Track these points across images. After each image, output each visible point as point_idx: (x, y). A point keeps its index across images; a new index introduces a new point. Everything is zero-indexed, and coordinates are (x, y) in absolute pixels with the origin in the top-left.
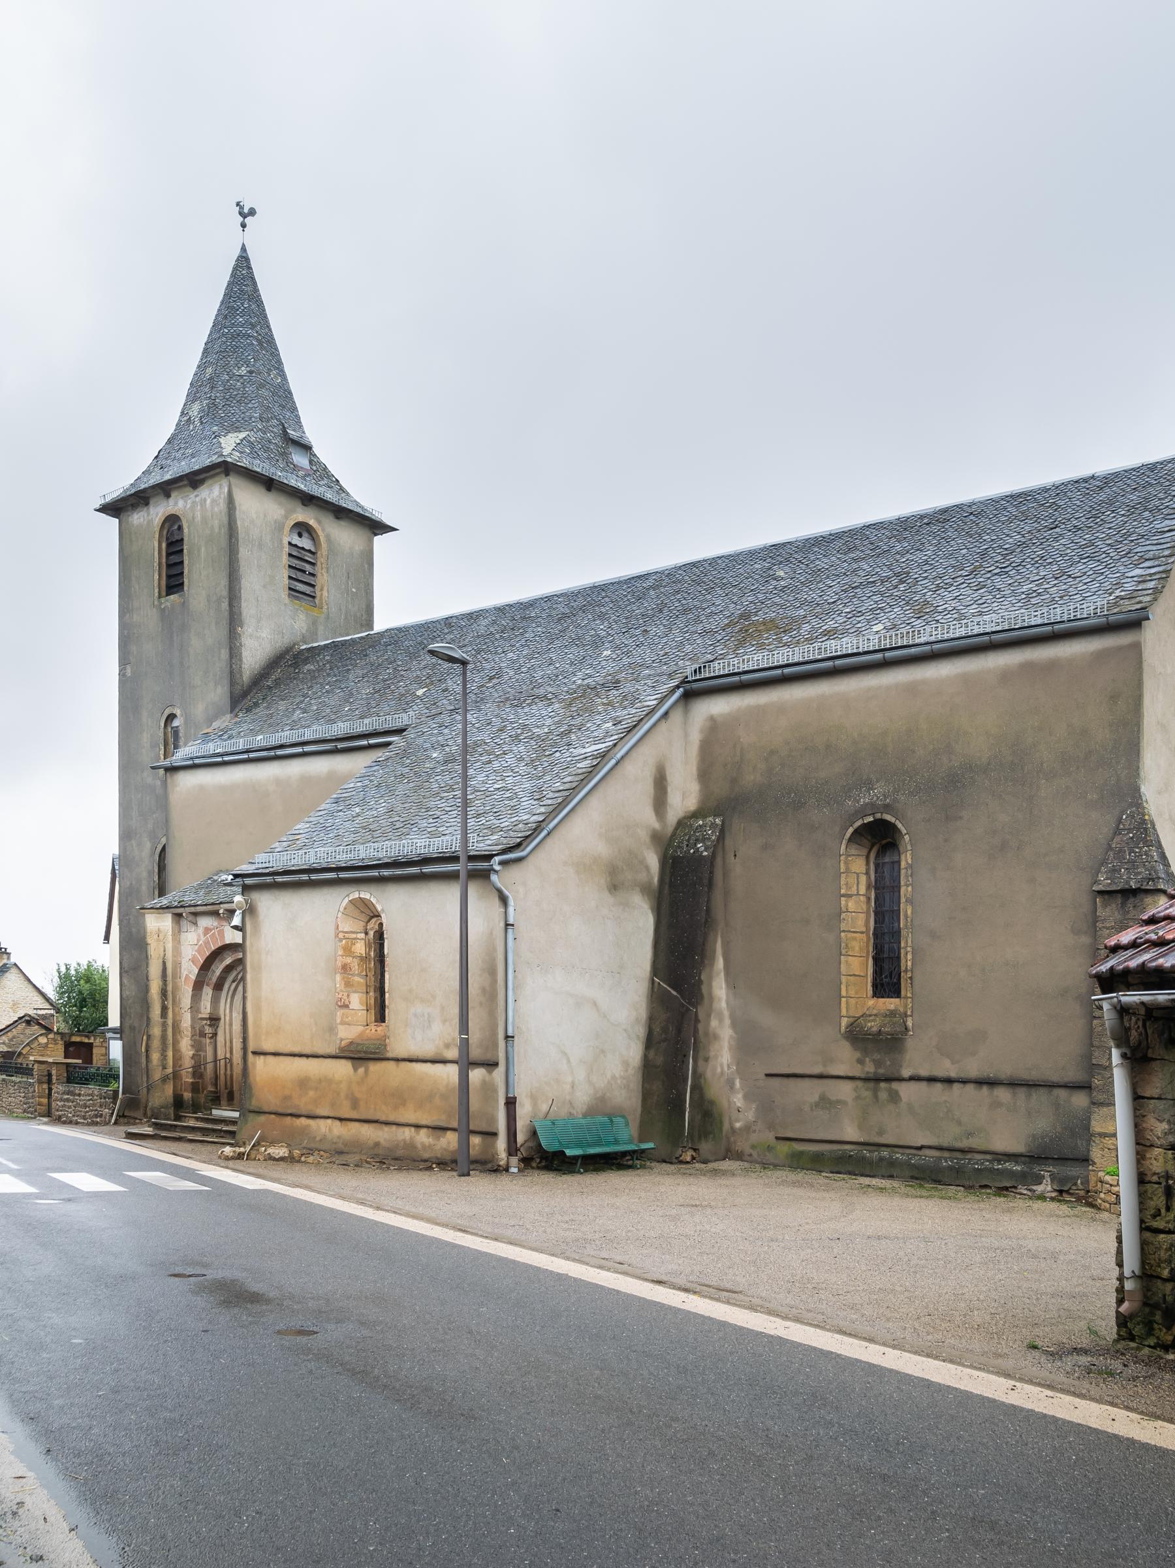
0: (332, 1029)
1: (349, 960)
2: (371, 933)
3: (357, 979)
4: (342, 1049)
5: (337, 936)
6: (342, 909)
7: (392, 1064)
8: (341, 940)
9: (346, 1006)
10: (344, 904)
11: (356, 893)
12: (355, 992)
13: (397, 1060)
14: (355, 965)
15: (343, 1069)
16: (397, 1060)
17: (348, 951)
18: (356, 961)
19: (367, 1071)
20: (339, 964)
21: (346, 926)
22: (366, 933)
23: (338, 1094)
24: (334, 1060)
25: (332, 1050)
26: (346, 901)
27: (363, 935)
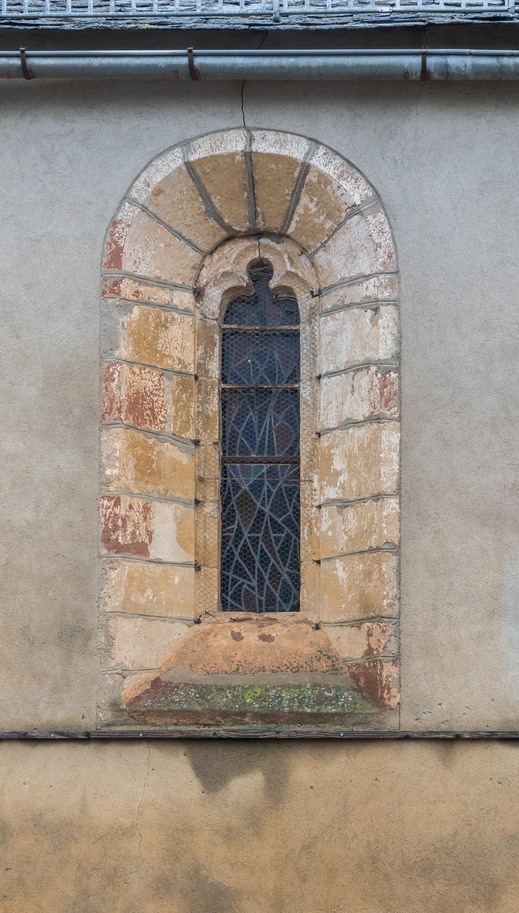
0: (75, 635)
1: (149, 381)
2: (215, 296)
3: (172, 452)
4: (134, 710)
5: (113, 289)
6: (141, 192)
7: (417, 759)
8: (126, 307)
9: (140, 549)
10: (158, 174)
11: (223, 137)
12: (166, 499)
13: (448, 740)
14: (167, 398)
15: (153, 785)
16: (448, 740)
17: (148, 352)
18: (169, 385)
19: (276, 788)
20: (122, 395)
21: (144, 257)
22: (198, 294)
23: (113, 878)
24: (86, 752)
25: (94, 715)
26: (175, 161)
27: (186, 299)
